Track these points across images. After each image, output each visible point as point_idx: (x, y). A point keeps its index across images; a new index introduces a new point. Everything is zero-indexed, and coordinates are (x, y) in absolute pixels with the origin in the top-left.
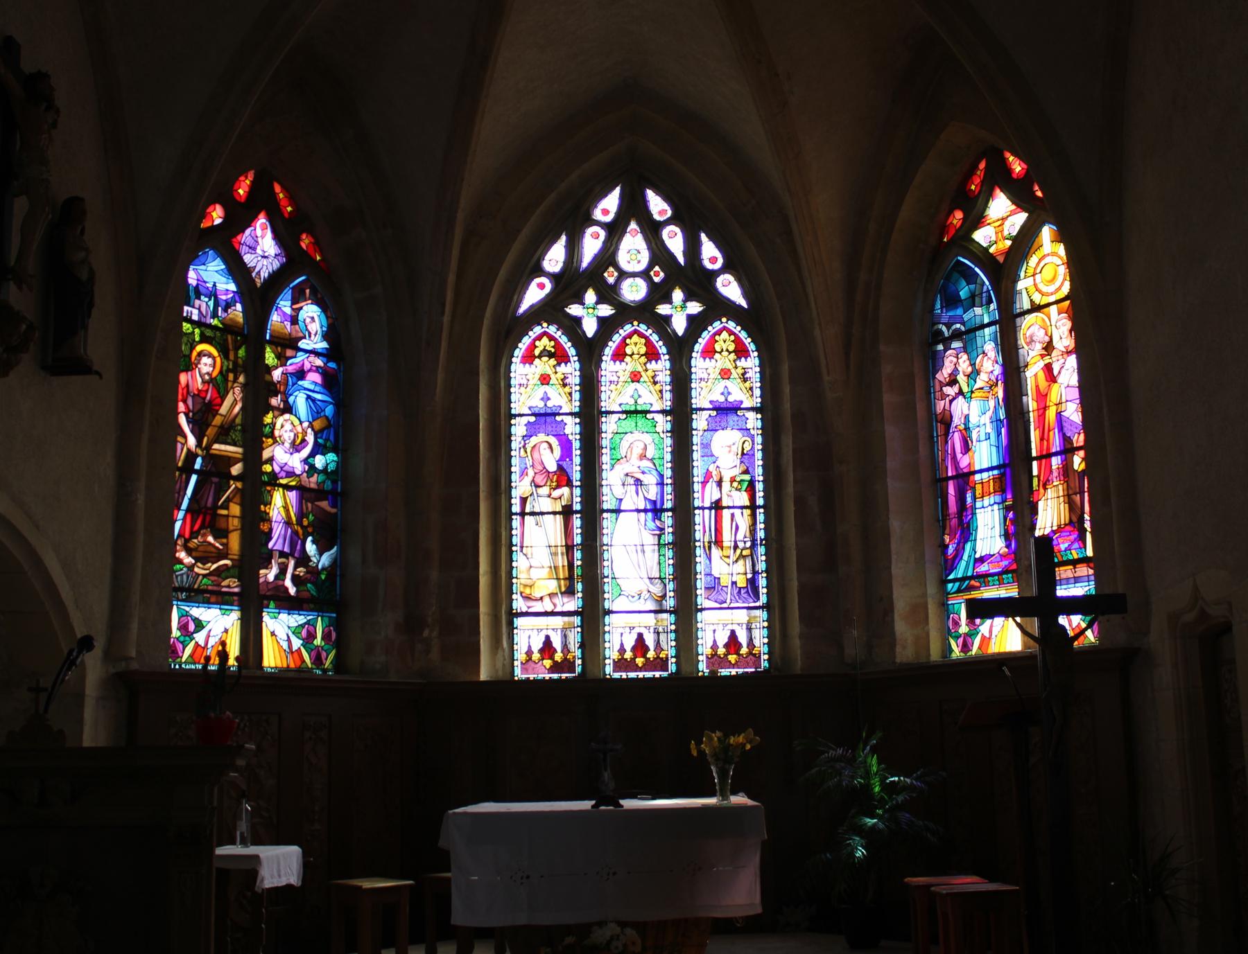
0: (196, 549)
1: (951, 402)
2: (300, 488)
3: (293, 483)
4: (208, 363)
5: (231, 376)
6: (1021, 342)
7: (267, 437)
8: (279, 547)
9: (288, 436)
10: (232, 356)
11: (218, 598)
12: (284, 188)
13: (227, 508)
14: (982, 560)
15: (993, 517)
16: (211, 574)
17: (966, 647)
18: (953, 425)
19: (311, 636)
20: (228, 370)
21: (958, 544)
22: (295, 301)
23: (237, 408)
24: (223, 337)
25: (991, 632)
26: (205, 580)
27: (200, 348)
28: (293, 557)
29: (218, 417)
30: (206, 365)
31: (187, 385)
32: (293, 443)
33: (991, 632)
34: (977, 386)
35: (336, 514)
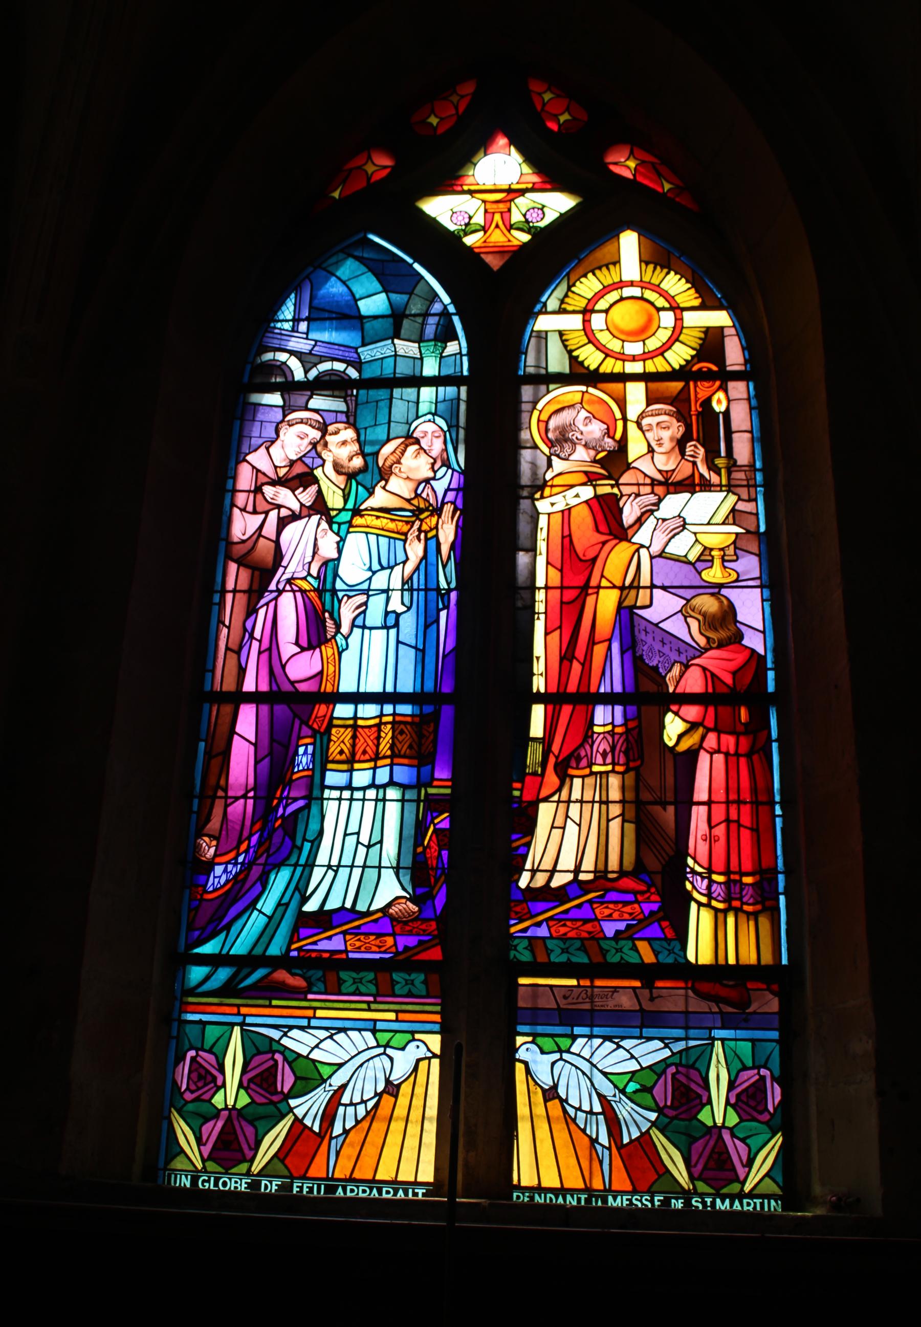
1: (283, 523)
6: (532, 432)
14: (324, 920)
15: (696, 393)
17: (231, 1148)
18: (282, 576)
21: (247, 867)
25: (328, 1117)
33: (328, 1117)
34: (372, 502)
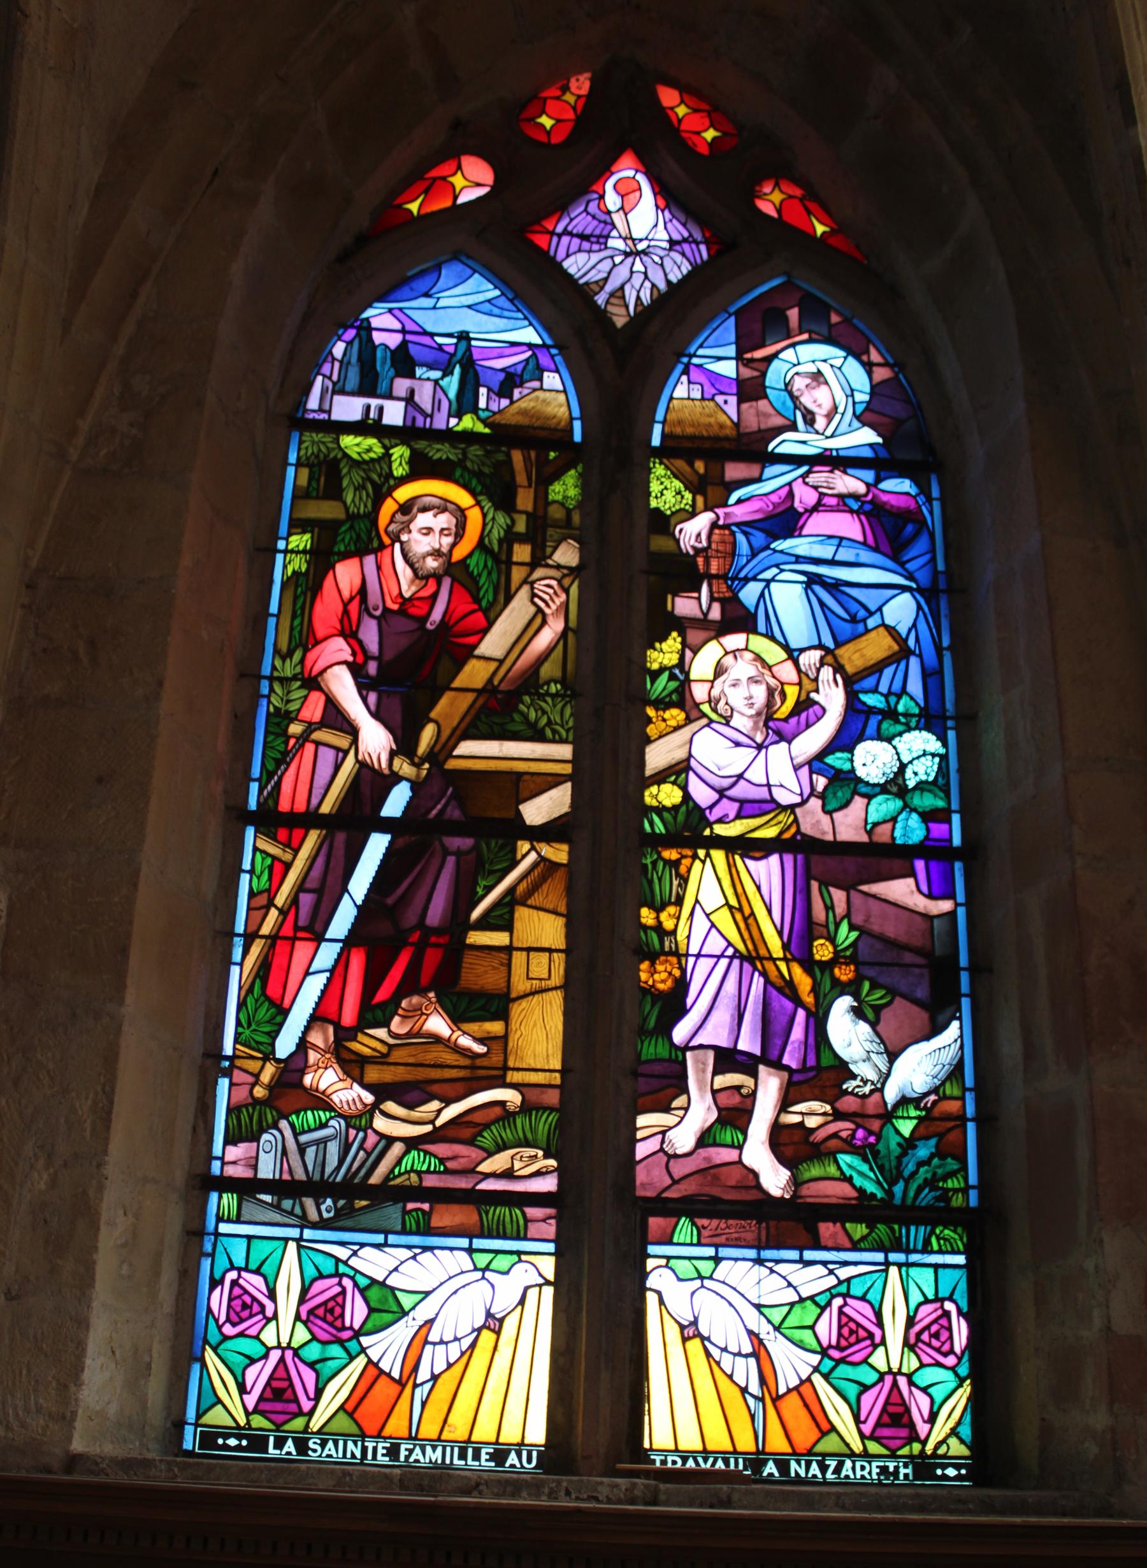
0: (382, 1060)
2: (797, 847)
3: (770, 832)
4: (433, 523)
5: (522, 552)
7: (662, 704)
8: (717, 1034)
9: (743, 695)
10: (525, 500)
11: (485, 1215)
12: (687, 91)
13: (507, 926)
16: (439, 1135)
19: (855, 1339)
20: (510, 538)
22: (744, 345)
23: (546, 638)
24: (498, 460)
26: (414, 1159)
27: (403, 493)
28: (777, 1065)
29: (472, 666)
30: (427, 535)
31: (363, 591)
32: (767, 716)
35: (952, 914)
